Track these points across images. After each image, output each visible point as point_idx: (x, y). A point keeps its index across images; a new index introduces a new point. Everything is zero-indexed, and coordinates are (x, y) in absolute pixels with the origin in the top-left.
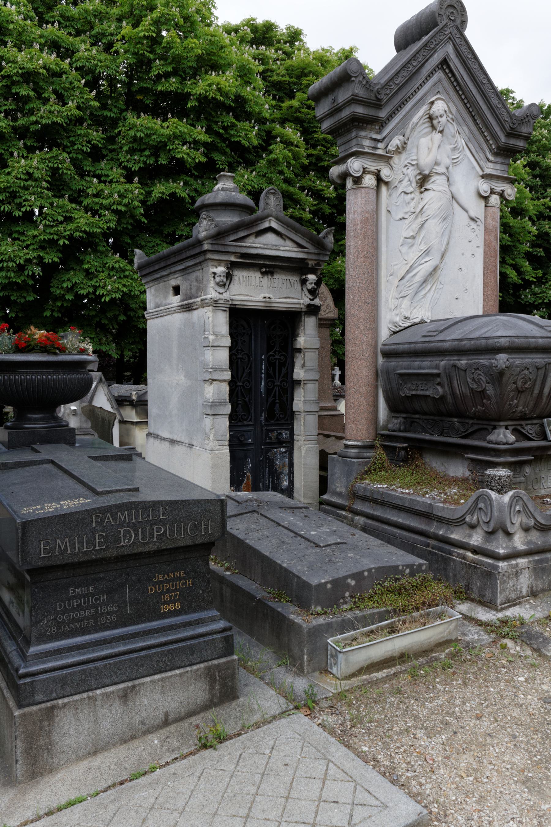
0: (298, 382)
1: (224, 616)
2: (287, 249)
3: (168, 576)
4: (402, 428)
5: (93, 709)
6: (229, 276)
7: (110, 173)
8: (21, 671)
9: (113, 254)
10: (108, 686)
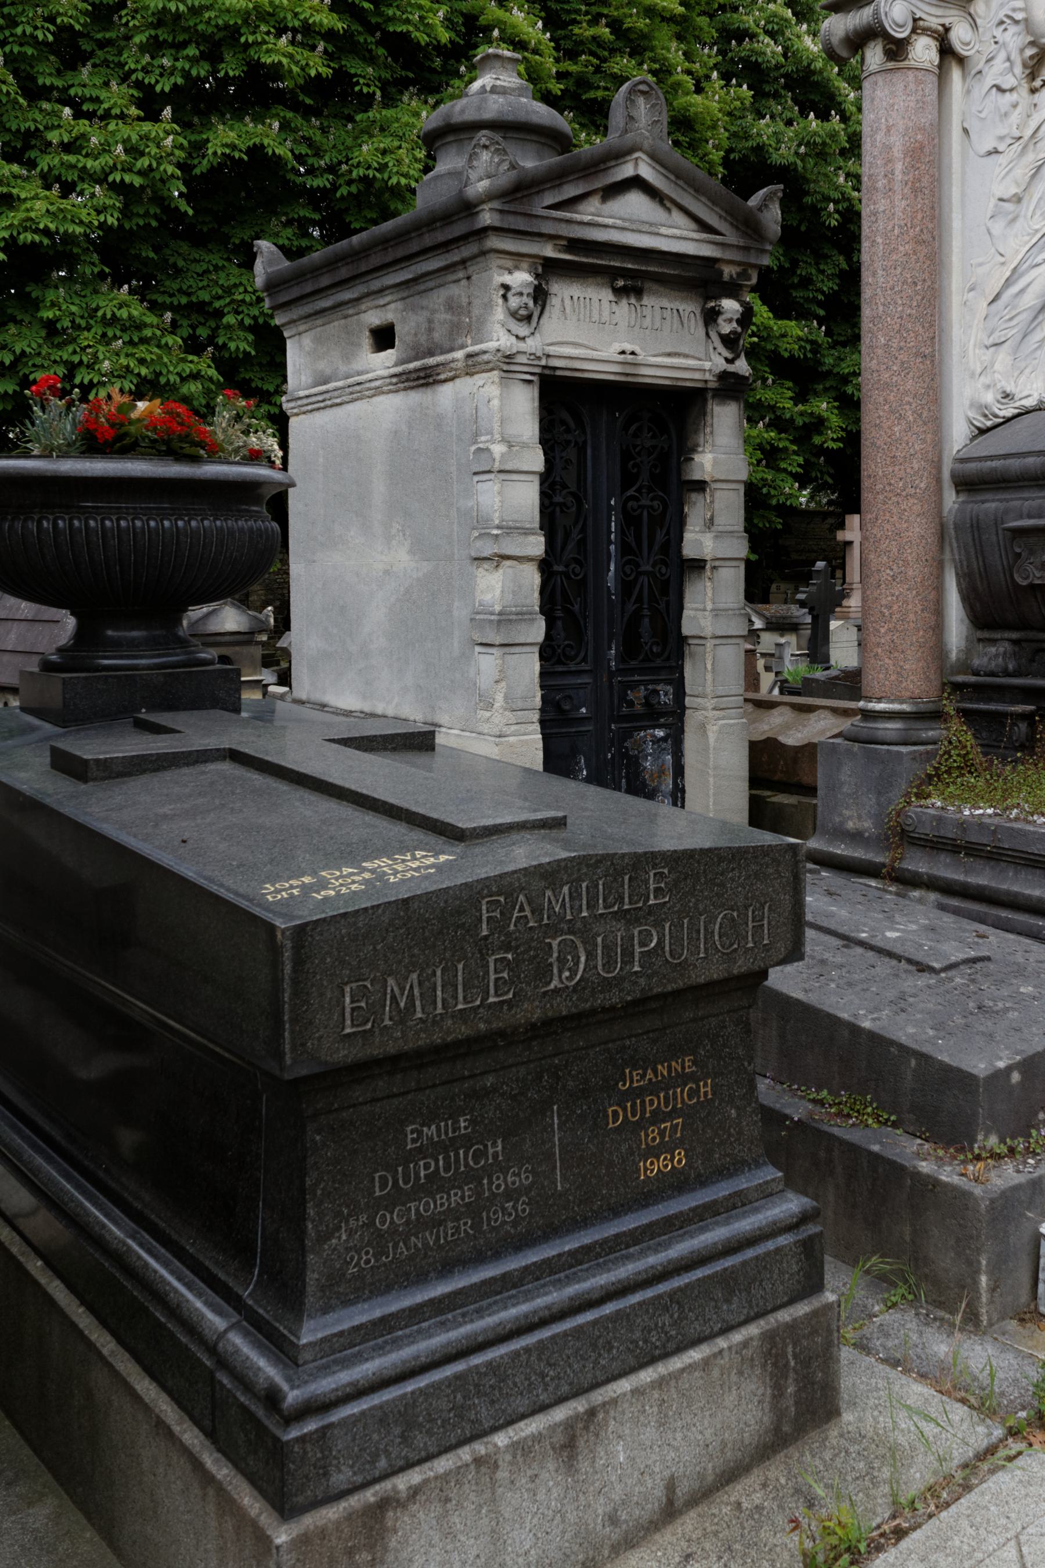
0: (698, 565)
1: (790, 1182)
2: (674, 235)
3: (655, 1071)
4: (1011, 667)
5: (488, 1494)
6: (540, 295)
7: (103, 94)
8: (293, 1396)
9: (111, 289)
10: (523, 1417)
